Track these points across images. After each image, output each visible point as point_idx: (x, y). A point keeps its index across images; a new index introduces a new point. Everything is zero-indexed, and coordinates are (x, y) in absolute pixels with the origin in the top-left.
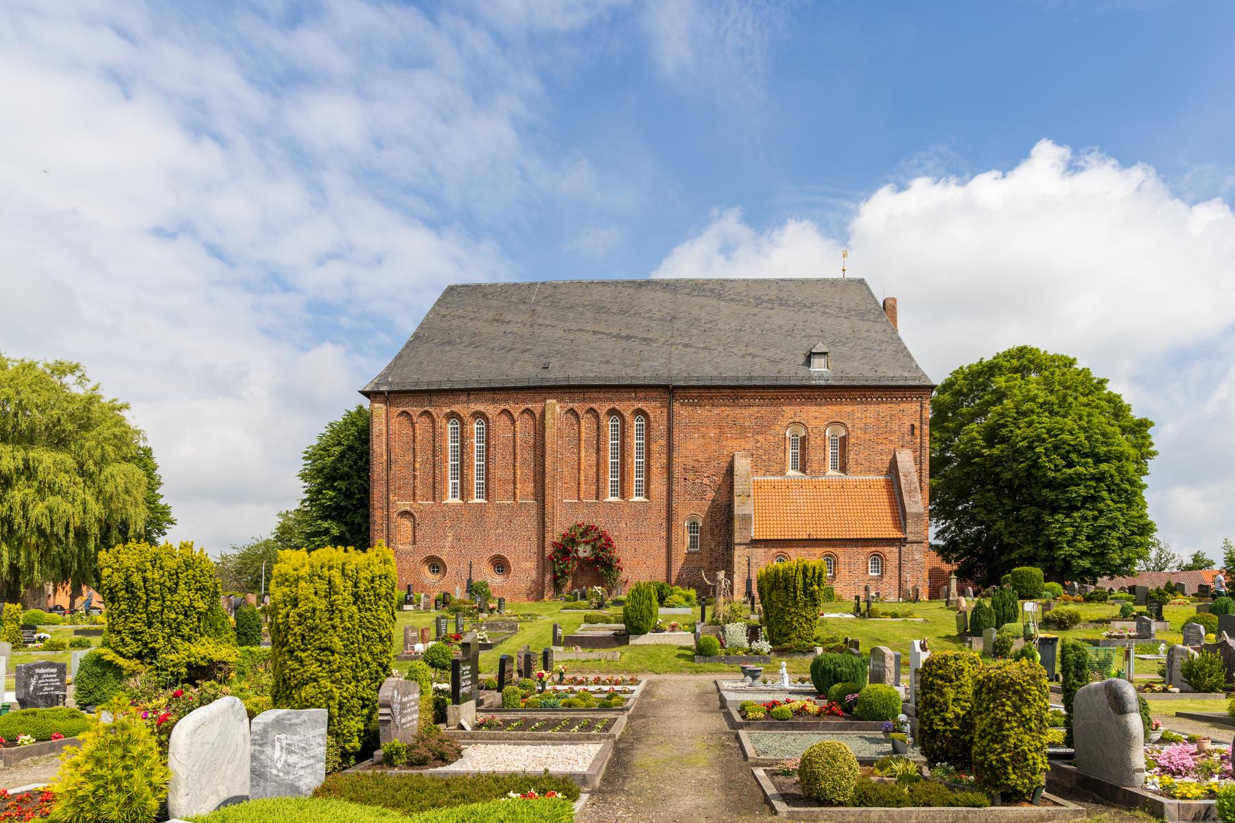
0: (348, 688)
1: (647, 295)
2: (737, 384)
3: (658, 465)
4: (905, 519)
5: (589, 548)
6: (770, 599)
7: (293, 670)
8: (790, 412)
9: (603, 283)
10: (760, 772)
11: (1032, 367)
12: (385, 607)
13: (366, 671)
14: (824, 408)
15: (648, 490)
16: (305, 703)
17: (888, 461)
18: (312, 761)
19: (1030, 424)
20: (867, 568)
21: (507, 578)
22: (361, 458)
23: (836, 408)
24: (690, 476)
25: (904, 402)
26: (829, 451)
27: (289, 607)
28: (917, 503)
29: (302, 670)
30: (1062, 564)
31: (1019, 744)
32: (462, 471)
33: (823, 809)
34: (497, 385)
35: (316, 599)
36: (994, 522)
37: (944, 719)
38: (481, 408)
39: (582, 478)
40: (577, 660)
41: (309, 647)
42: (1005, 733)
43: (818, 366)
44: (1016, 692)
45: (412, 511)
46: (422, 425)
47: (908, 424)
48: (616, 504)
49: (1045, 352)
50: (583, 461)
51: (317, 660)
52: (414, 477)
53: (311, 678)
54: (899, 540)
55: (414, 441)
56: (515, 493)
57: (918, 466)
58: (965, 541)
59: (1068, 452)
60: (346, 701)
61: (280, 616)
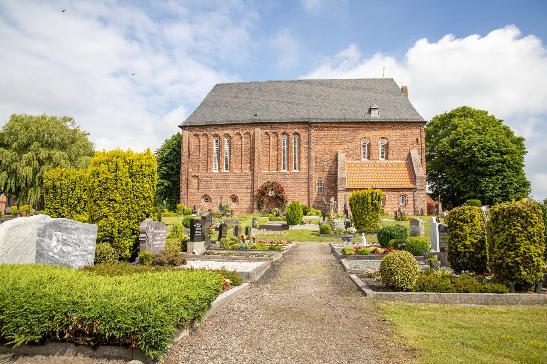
0: (123, 222)
1: (299, 86)
2: (338, 121)
3: (304, 156)
4: (415, 180)
5: (273, 192)
6: (355, 208)
7: (95, 211)
8: (362, 133)
9: (280, 81)
10: (354, 276)
11: (469, 115)
12: (148, 182)
13: (135, 214)
14: (377, 132)
15: (299, 167)
16: (100, 229)
17: (407, 154)
18: (84, 253)
19: (470, 138)
20: (399, 201)
21: (237, 205)
22: (178, 154)
23: (383, 132)
24: (318, 161)
25: (413, 129)
26: (380, 150)
27: (96, 177)
28: (421, 172)
29: (100, 211)
30: (488, 200)
31: (527, 251)
32: (219, 161)
33: (397, 293)
34: (235, 123)
35: (108, 173)
36: (456, 182)
37: (464, 245)
38: (228, 132)
39: (271, 162)
40: (264, 235)
41: (104, 199)
42: (517, 244)
43: (374, 114)
44: (523, 217)
45: (198, 175)
46: (203, 140)
47: (415, 139)
48: (285, 173)
49: (474, 109)
50: (271, 154)
51: (108, 206)
52: (199, 161)
53: (104, 216)
54: (413, 188)
55: (199, 146)
56: (241, 168)
57: (420, 157)
58: (442, 191)
59: (488, 150)
60: (122, 229)
61: (91, 182)
